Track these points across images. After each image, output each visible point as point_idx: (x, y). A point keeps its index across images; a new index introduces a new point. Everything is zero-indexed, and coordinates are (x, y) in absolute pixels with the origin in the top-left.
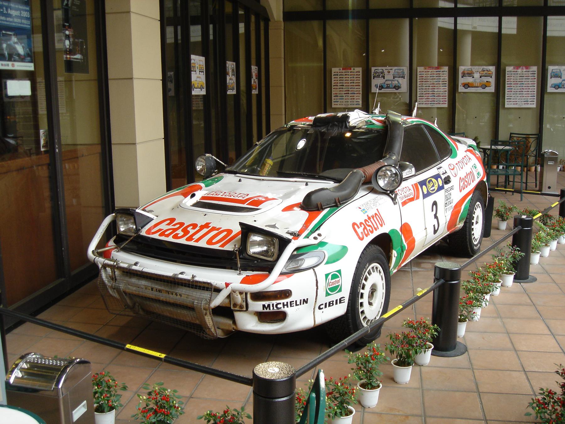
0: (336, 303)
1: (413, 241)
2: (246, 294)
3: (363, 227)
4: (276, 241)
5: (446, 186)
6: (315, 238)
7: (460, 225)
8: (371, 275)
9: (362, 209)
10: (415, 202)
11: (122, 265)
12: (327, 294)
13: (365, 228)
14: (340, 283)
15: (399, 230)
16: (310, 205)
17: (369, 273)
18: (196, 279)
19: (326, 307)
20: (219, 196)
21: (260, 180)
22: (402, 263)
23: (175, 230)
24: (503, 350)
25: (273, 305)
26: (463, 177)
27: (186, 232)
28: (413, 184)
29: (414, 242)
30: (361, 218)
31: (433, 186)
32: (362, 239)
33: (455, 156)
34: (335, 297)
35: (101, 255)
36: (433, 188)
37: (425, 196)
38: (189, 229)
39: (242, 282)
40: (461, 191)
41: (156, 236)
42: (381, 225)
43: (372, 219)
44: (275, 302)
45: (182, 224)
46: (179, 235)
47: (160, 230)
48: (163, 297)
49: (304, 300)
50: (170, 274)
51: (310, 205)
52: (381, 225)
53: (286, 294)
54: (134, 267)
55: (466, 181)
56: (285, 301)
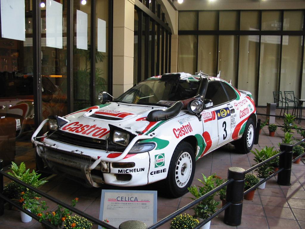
0: (161, 172)
1: (211, 142)
2: (110, 163)
3: (179, 131)
4: (128, 135)
5: (232, 114)
6: (151, 135)
7: (240, 136)
8: (184, 158)
9: (180, 121)
10: (213, 121)
11: (47, 145)
12: (156, 167)
13: (180, 132)
14: (164, 161)
15: (202, 135)
16: (151, 119)
18: (83, 154)
19: (155, 173)
20: (104, 112)
21: (129, 105)
23: (77, 128)
24: (258, 204)
25: (124, 170)
27: (83, 129)
28: (212, 111)
29: (212, 142)
30: (179, 126)
31: (224, 113)
32: (178, 137)
33: (239, 99)
34: (160, 168)
35: (38, 140)
36: (224, 114)
37: (219, 118)
38: (85, 128)
40: (240, 118)
41: (67, 131)
42: (190, 131)
43: (185, 128)
44: (125, 169)
45: (81, 125)
46: (79, 131)
47: (70, 128)
48: (66, 163)
49: (142, 169)
50: (70, 151)
51: (151, 119)
52: (190, 131)
53: (132, 165)
54: (53, 147)
55: (244, 113)
56: (131, 169)
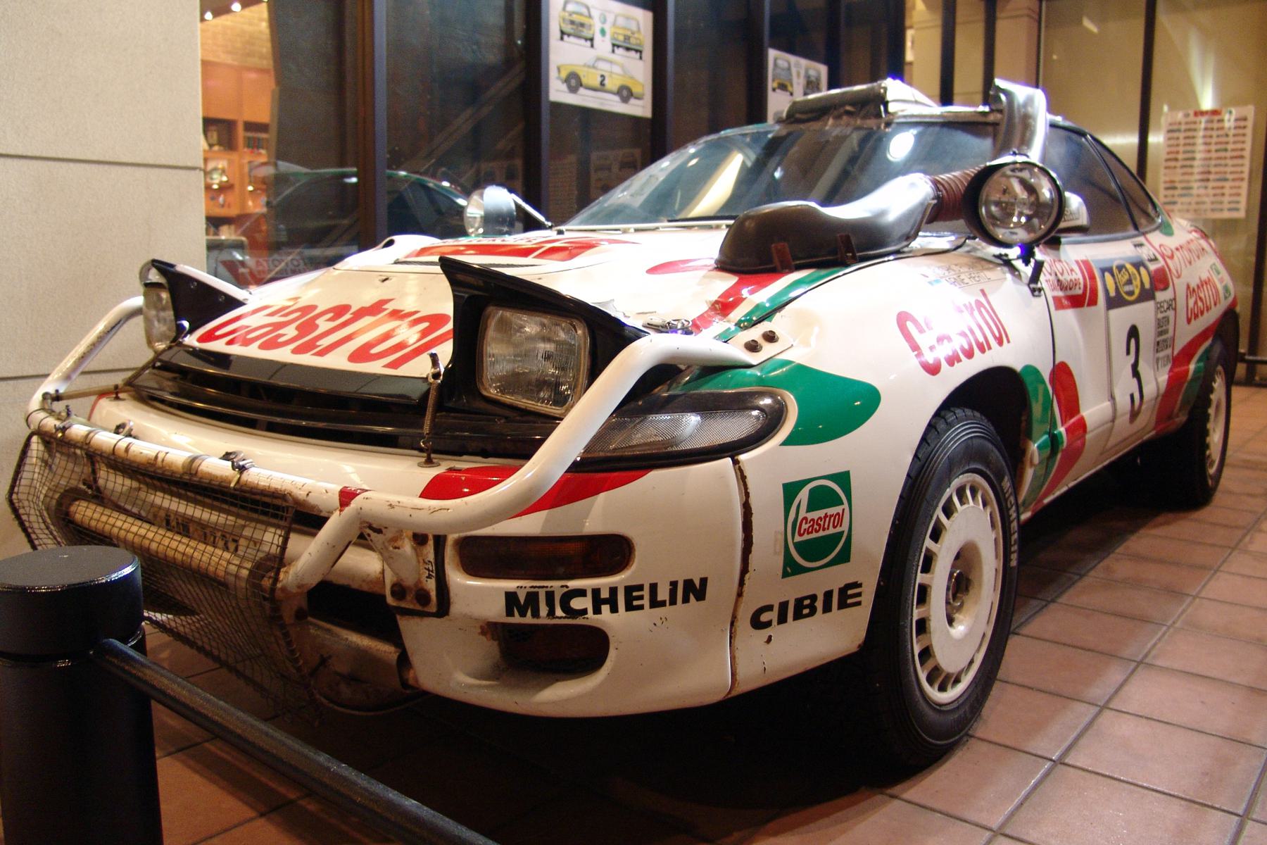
2: (440, 541)
7: (1182, 418)
12: (791, 569)
14: (845, 527)
17: (949, 510)
22: (1046, 495)
26: (1194, 283)
34: (830, 578)
39: (428, 493)
49: (689, 584)
53: (610, 551)
56: (603, 583)
